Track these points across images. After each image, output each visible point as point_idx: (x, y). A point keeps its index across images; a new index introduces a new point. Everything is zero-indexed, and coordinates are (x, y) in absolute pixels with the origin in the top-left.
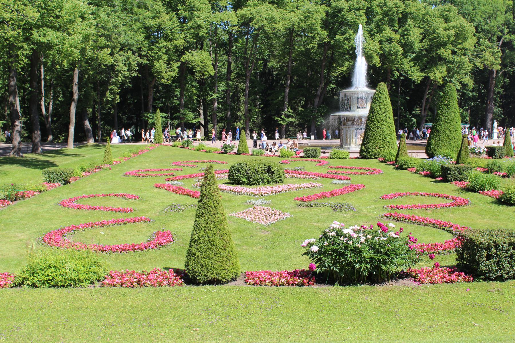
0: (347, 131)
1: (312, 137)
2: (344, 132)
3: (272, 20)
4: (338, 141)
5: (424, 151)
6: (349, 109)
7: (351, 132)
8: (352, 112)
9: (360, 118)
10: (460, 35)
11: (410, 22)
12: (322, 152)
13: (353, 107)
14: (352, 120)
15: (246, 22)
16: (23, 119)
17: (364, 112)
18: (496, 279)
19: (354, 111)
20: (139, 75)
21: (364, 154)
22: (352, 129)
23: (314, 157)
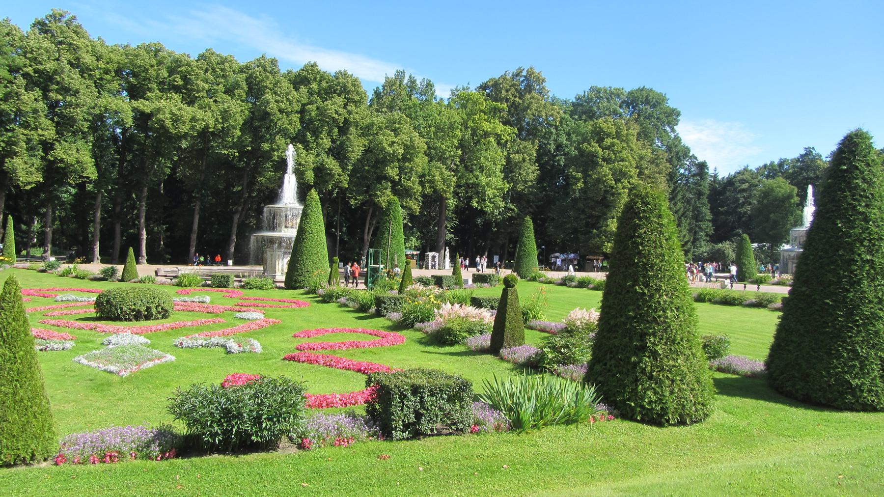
0: (272, 255)
1: (230, 262)
2: (268, 255)
3: (176, 120)
4: (261, 268)
5: (364, 281)
6: (273, 228)
7: (277, 257)
8: (276, 232)
9: (290, 239)
10: (409, 149)
11: (352, 129)
12: (236, 281)
13: (280, 226)
14: (280, 241)
15: (142, 118)
16: (255, 440)
17: (290, 233)
18: (126, 320)
19: (280, 231)
20: (608, 273)
21: (291, 283)
22: (279, 253)
23: (225, 287)
